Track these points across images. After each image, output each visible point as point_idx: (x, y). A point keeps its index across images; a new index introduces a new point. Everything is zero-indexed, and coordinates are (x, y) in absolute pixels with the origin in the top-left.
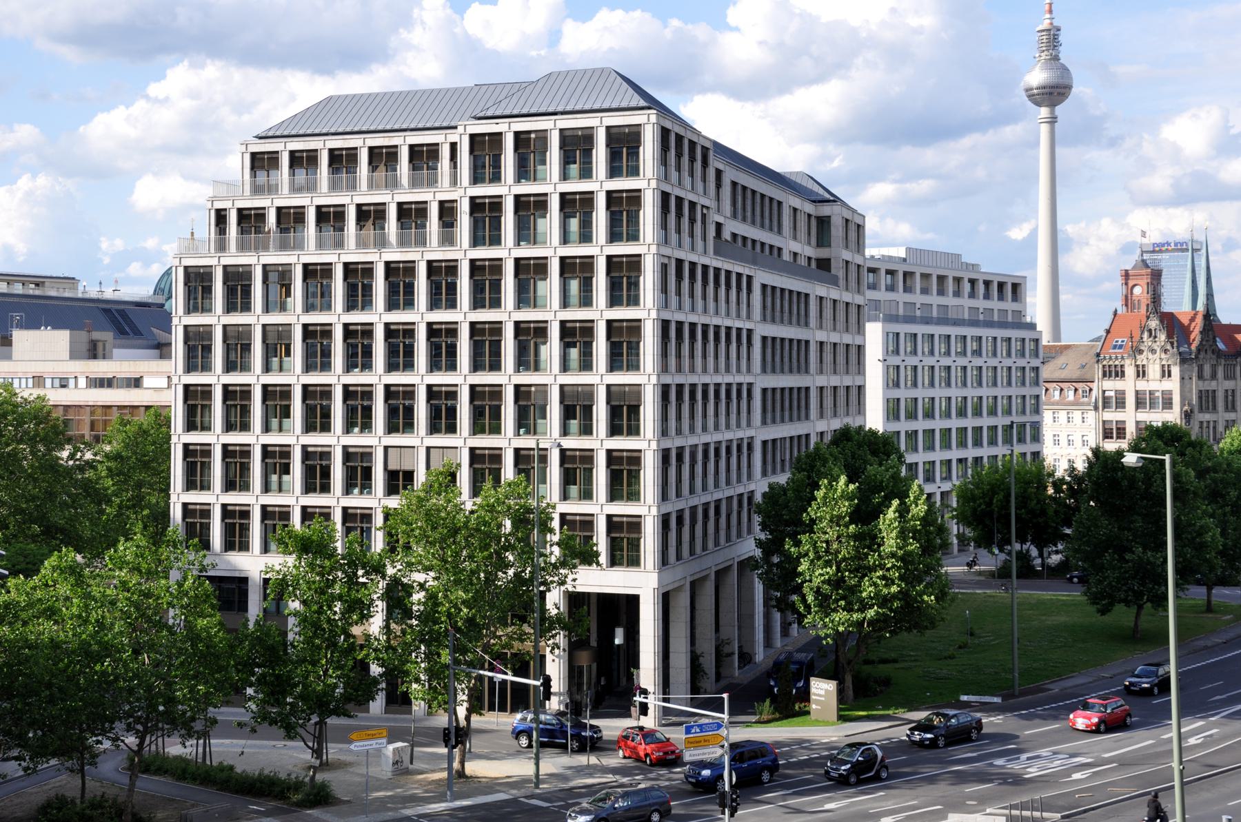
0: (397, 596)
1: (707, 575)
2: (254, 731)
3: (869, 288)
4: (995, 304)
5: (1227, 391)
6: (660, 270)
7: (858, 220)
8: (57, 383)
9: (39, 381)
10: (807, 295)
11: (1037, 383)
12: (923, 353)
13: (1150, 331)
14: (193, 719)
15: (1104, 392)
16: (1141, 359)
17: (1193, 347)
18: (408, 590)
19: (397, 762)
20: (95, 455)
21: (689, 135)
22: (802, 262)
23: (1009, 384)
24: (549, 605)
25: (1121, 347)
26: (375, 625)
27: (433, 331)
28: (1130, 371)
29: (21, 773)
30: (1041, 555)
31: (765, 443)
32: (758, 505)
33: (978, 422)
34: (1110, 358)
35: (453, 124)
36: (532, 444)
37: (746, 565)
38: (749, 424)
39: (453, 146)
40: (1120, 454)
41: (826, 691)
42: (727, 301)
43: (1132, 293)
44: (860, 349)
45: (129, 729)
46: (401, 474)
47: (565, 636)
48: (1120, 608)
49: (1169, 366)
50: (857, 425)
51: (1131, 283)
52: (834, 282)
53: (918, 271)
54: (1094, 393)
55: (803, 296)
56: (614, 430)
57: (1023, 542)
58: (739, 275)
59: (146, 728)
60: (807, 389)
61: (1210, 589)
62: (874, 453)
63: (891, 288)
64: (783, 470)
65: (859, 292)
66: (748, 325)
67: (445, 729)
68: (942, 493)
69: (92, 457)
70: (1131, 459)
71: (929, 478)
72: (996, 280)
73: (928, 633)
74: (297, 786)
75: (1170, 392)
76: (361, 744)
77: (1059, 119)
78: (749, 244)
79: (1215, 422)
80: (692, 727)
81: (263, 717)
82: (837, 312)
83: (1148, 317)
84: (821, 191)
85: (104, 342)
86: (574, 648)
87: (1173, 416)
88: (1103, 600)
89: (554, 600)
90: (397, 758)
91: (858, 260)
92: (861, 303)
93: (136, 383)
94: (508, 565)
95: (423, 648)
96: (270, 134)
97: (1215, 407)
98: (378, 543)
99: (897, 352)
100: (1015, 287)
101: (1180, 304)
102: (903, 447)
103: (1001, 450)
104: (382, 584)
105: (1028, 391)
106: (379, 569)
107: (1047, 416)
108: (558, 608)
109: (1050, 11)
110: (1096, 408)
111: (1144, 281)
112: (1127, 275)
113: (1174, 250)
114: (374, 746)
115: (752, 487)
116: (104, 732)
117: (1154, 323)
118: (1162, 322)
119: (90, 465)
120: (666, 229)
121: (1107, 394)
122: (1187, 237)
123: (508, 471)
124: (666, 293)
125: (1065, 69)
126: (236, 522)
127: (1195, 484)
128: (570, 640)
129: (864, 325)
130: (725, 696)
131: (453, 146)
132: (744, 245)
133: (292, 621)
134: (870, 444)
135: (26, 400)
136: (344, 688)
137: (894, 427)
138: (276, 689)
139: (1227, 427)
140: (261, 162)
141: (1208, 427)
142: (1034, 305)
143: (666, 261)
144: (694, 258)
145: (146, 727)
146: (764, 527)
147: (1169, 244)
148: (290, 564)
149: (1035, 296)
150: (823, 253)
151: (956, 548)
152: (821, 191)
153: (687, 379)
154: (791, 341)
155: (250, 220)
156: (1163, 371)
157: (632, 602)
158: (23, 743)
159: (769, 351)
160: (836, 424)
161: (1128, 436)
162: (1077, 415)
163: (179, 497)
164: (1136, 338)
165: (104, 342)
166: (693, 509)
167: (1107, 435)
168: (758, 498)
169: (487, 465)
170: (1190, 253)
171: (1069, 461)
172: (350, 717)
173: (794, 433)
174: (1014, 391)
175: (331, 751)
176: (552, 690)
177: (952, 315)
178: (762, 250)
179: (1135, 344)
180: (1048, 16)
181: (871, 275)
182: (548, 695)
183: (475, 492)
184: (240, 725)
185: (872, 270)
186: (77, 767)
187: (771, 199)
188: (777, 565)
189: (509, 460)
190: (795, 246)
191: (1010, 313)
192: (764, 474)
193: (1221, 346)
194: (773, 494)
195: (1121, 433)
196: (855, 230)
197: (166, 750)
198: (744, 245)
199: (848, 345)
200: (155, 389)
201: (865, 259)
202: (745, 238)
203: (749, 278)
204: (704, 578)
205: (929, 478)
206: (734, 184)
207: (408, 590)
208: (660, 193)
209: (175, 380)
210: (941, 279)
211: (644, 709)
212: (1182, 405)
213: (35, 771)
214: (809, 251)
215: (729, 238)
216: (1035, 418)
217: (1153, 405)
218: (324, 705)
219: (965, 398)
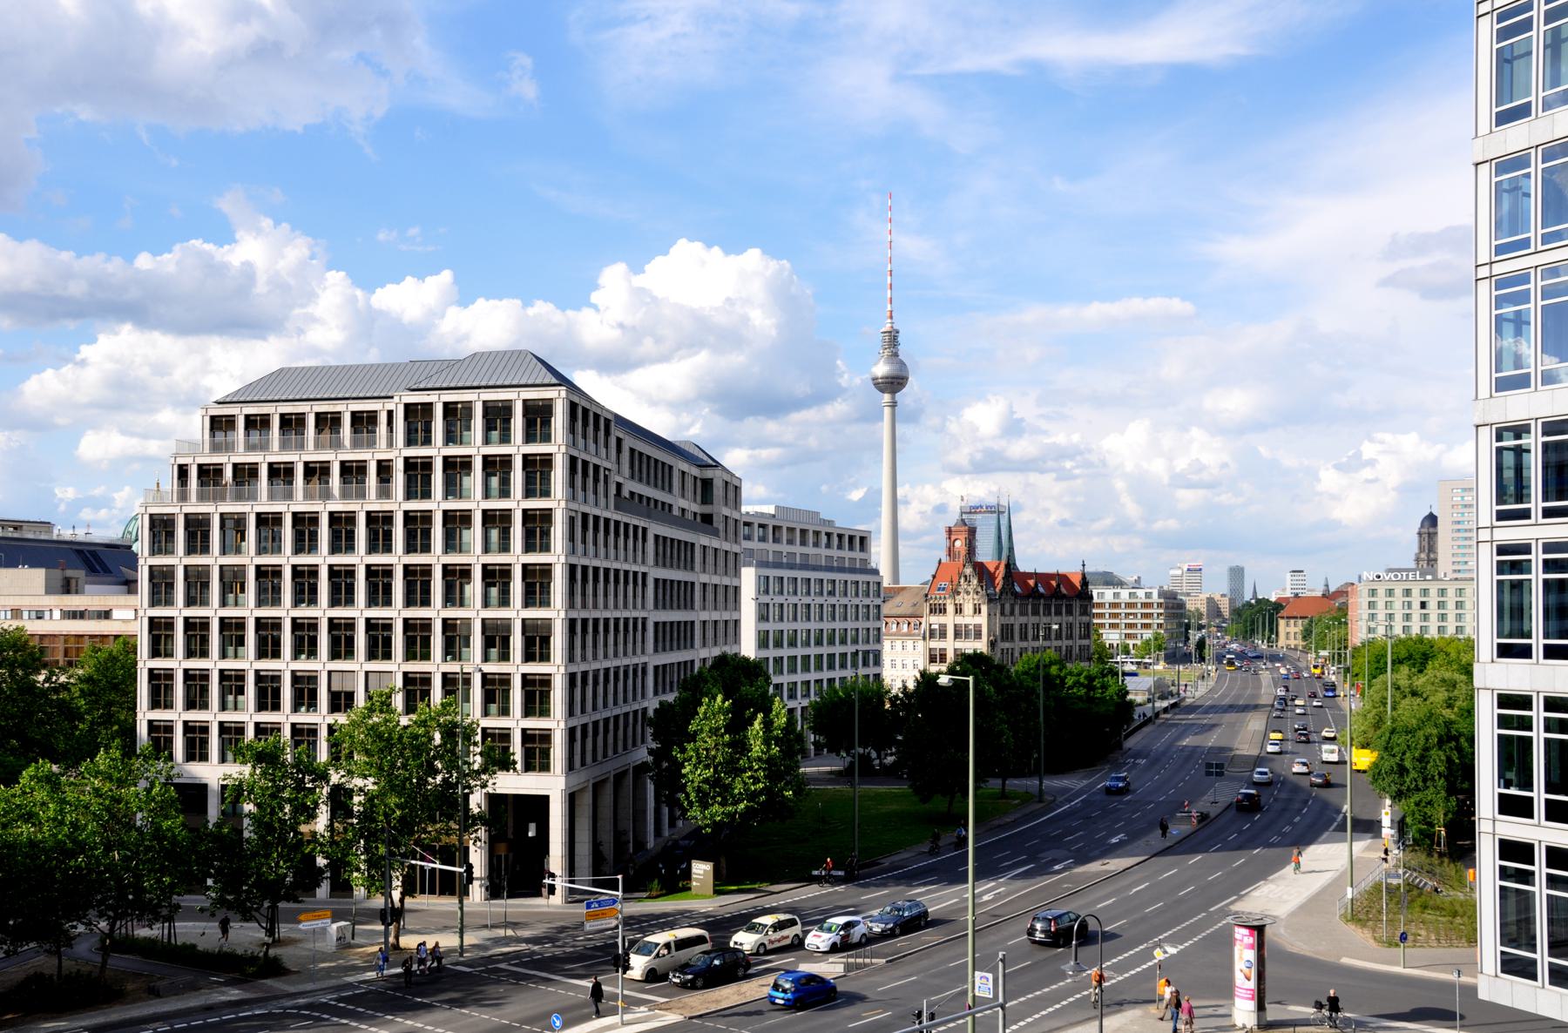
0: (340, 798)
3: (745, 539)
4: (846, 554)
8: (33, 615)
10: (693, 545)
11: (879, 618)
12: (788, 592)
13: (966, 576)
15: (930, 625)
16: (959, 599)
17: (997, 590)
18: (350, 793)
22: (689, 516)
23: (857, 619)
25: (944, 589)
26: (321, 822)
28: (950, 609)
30: (879, 757)
31: (656, 668)
33: (831, 650)
37: (641, 769)
39: (390, 413)
42: (626, 549)
44: (737, 589)
51: (953, 537)
52: (715, 533)
53: (785, 525)
54: (923, 626)
58: (636, 527)
63: (763, 539)
68: (802, 708)
71: (792, 696)
74: (253, 959)
75: (980, 626)
84: (705, 458)
87: (981, 646)
89: (477, 801)
91: (736, 515)
92: (738, 551)
93: (106, 615)
98: (323, 755)
99: (767, 592)
100: (863, 540)
102: (771, 671)
104: (326, 790)
105: (871, 624)
106: (324, 777)
107: (887, 644)
109: (891, 317)
110: (924, 638)
111: (965, 535)
112: (950, 531)
113: (985, 512)
117: (968, 571)
118: (974, 569)
121: (933, 627)
122: (992, 501)
125: (902, 364)
127: (994, 698)
131: (390, 413)
133: (246, 821)
137: (764, 654)
138: (230, 881)
139: (1021, 655)
140: (220, 424)
142: (878, 553)
146: (655, 737)
149: (879, 546)
150: (707, 509)
152: (705, 458)
155: (209, 474)
156: (975, 609)
157: (543, 801)
160: (716, 652)
161: (948, 661)
162: (909, 644)
163: (145, 715)
164: (955, 583)
167: (932, 660)
170: (995, 515)
174: (861, 625)
177: (811, 562)
180: (889, 321)
182: (470, 879)
185: (747, 524)
190: (683, 503)
191: (798, 556)
192: (656, 693)
193: (1018, 589)
195: (943, 658)
200: (124, 621)
203: (645, 530)
204: (604, 781)
205: (792, 696)
206: (632, 450)
207: (350, 793)
209: (141, 613)
212: (989, 635)
213: (15, 952)
214: (694, 507)
216: (876, 647)
218: (274, 891)
219: (822, 630)
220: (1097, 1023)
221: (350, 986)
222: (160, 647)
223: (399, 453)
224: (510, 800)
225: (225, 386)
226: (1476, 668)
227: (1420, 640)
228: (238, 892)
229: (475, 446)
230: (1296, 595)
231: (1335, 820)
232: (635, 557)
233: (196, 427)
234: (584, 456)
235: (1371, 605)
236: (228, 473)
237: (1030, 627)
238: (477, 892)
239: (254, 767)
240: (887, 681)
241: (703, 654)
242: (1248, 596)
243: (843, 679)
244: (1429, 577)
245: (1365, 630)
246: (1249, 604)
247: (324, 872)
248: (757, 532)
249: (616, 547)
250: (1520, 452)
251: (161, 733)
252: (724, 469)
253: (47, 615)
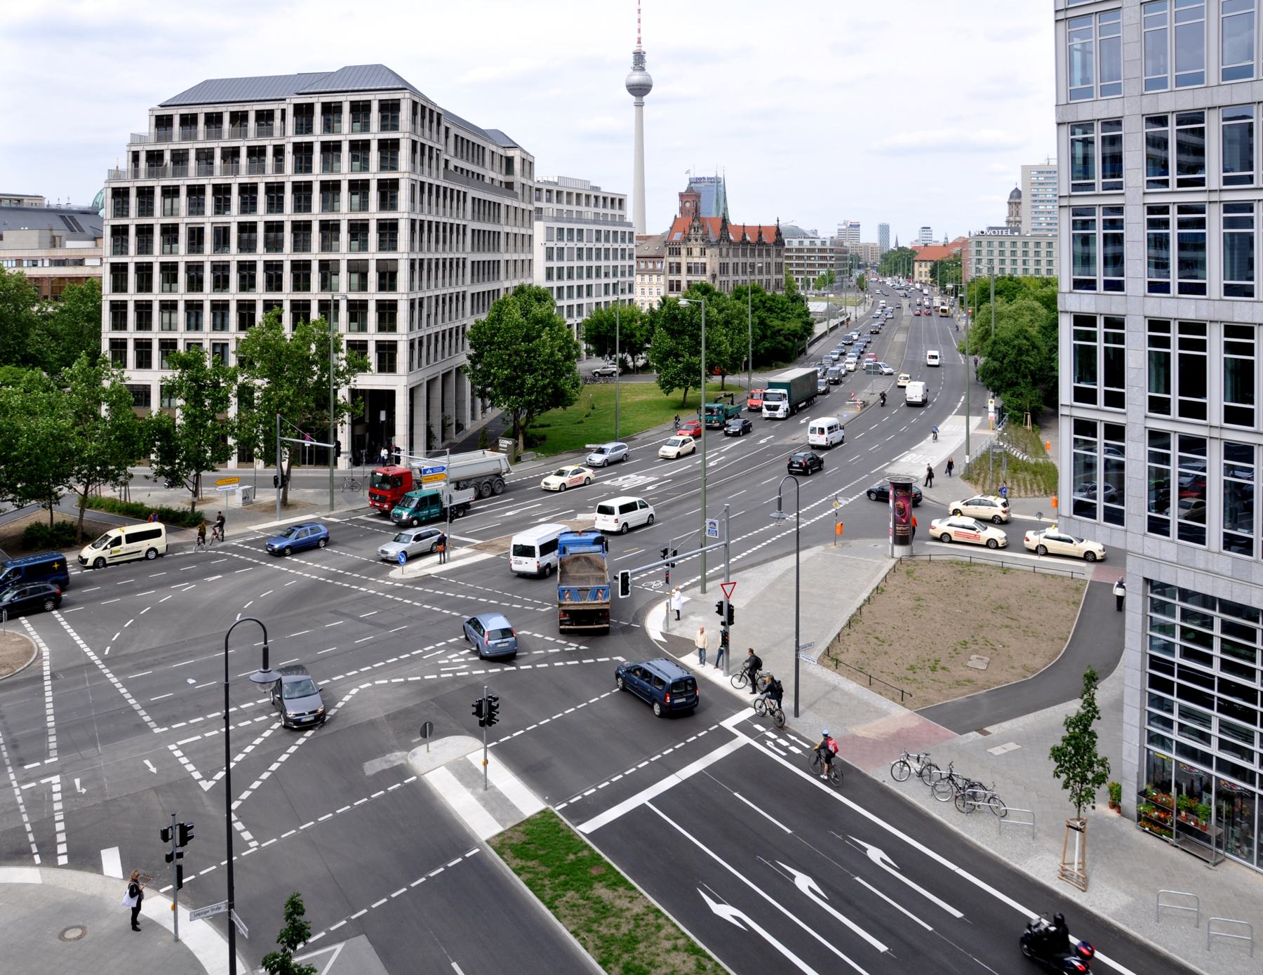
0: (245, 394)
4: (609, 211)
8: (31, 263)
9: (19, 262)
10: (499, 204)
14: (119, 475)
16: (690, 245)
18: (252, 391)
22: (497, 184)
24: (339, 397)
26: (232, 411)
27: (296, 265)
30: (633, 360)
31: (473, 295)
36: (329, 297)
37: (459, 371)
39: (283, 111)
42: (451, 208)
48: (676, 390)
52: (515, 196)
56: (382, 288)
58: (459, 192)
59: (89, 480)
60: (499, 261)
62: (539, 300)
74: (184, 514)
78: (465, 172)
81: (160, 473)
86: (354, 424)
87: (705, 279)
88: (668, 385)
89: (343, 394)
91: (530, 183)
93: (80, 262)
98: (233, 362)
100: (621, 201)
101: (710, 213)
104: (235, 387)
106: (234, 379)
115: (465, 322)
116: (63, 483)
122: (714, 176)
123: (315, 315)
126: (143, 348)
131: (283, 111)
132: (462, 172)
133: (178, 412)
134: (536, 295)
137: (550, 284)
138: (168, 455)
140: (163, 122)
144: (431, 181)
146: (472, 346)
150: (509, 179)
155: (155, 158)
157: (391, 394)
158: (12, 489)
160: (516, 283)
163: (108, 333)
166: (429, 336)
167: (671, 289)
169: (300, 309)
172: (214, 471)
182: (338, 453)
183: (294, 327)
184: (147, 477)
185: (538, 190)
187: (479, 146)
188: (479, 370)
189: (315, 307)
190: (493, 175)
192: (472, 313)
194: (478, 328)
196: (528, 164)
200: (92, 266)
202: (462, 169)
203: (465, 193)
204: (435, 379)
206: (456, 136)
207: (252, 391)
209: (105, 260)
213: (22, 507)
214: (501, 177)
217: (696, 272)
218: (199, 464)
220: (795, 555)
221: (253, 533)
222: (119, 286)
223: (291, 139)
224: (368, 393)
225: (168, 95)
226: (1060, 298)
227: (1011, 279)
228: (172, 464)
229: (346, 132)
230: (926, 245)
231: (955, 407)
232: (458, 213)
233: (146, 127)
234: (420, 140)
235: (979, 252)
236: (167, 156)
237: (740, 265)
238: (343, 463)
239: (183, 372)
240: (639, 304)
241: (506, 284)
242: (892, 246)
244: (1016, 234)
245: (974, 270)
246: (893, 251)
247: (232, 449)
249: (444, 207)
250: (1087, 143)
251: (118, 347)
252: (522, 150)
253: (40, 263)
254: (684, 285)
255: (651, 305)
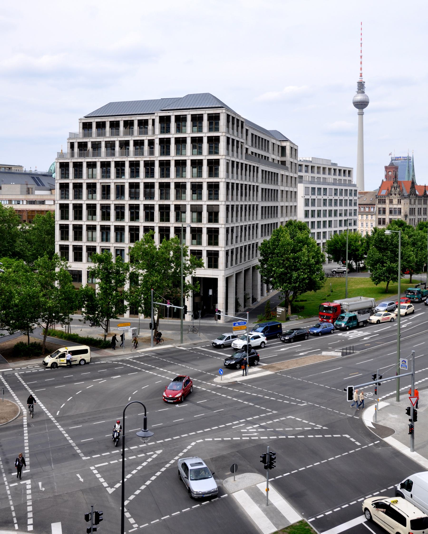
0: (134, 278)
1: (242, 271)
2: (85, 323)
5: (419, 208)
6: (226, 164)
7: (296, 148)
8: (16, 202)
9: (10, 201)
10: (277, 174)
14: (65, 318)
16: (391, 197)
18: (137, 276)
19: (134, 334)
20: (29, 228)
21: (237, 117)
22: (276, 162)
26: (127, 287)
29: (8, 334)
31: (262, 225)
32: (260, 247)
34: (381, 197)
35: (153, 112)
38: (257, 219)
39: (153, 120)
40: (384, 230)
41: (282, 311)
42: (250, 176)
43: (388, 174)
45: (43, 321)
46: (213, 213)
47: (192, 292)
49: (400, 199)
50: (294, 219)
52: (287, 169)
55: (276, 174)
56: (210, 221)
57: (350, 260)
59: (49, 321)
60: (277, 207)
61: (411, 276)
62: (300, 229)
64: (268, 235)
65: (296, 173)
66: (257, 184)
67: (150, 323)
68: (323, 243)
69: (28, 228)
70: (388, 232)
72: (343, 169)
73: (317, 291)
76: (122, 328)
77: (364, 113)
78: (257, 155)
79: (415, 219)
80: (236, 323)
82: (288, 180)
83: (394, 183)
85: (32, 188)
87: (400, 217)
88: (377, 279)
89: (188, 279)
90: (134, 333)
91: (295, 161)
94: (172, 268)
95: (142, 295)
96: (89, 116)
97: (414, 214)
98: (127, 259)
100: (349, 172)
101: (404, 178)
103: (343, 228)
108: (189, 282)
114: (126, 329)
116: (35, 322)
119: (27, 232)
120: (228, 150)
123: (172, 235)
124: (228, 173)
126: (78, 250)
127: (408, 240)
128: (193, 293)
129: (297, 184)
130: (248, 313)
131: (153, 120)
132: (256, 155)
134: (299, 227)
135: (6, 208)
136: (115, 309)
137: (307, 220)
138: (91, 309)
140: (87, 126)
141: (412, 221)
143: (228, 161)
144: (238, 160)
145: (50, 320)
146: (262, 255)
147: (400, 157)
148: (96, 266)
150: (283, 159)
151: (327, 262)
153: (235, 203)
154: (272, 190)
155: (83, 146)
158: (8, 324)
159: (264, 193)
160: (287, 219)
163: (58, 242)
165: (32, 188)
166: (237, 248)
167: (380, 223)
168: (259, 245)
169: (164, 232)
171: (366, 232)
173: (272, 222)
175: (111, 330)
176: (187, 310)
178: (262, 158)
179: (389, 192)
181: (300, 167)
182: (186, 312)
183: (161, 242)
184: (80, 320)
185: (300, 165)
186: (26, 333)
189: (172, 231)
191: (347, 181)
192: (262, 236)
195: (384, 223)
196: (294, 151)
197: (55, 328)
198: (256, 155)
199: (291, 191)
200: (49, 205)
201: (298, 161)
203: (257, 168)
204: (241, 272)
206: (252, 134)
207: (137, 276)
208: (226, 115)
209: (56, 202)
210: (324, 168)
211: (219, 317)
213: (13, 333)
214: (279, 158)
215: (250, 153)
217: (395, 213)
243: (340, 231)
248: (304, 168)
254: (387, 221)
255: (367, 232)
